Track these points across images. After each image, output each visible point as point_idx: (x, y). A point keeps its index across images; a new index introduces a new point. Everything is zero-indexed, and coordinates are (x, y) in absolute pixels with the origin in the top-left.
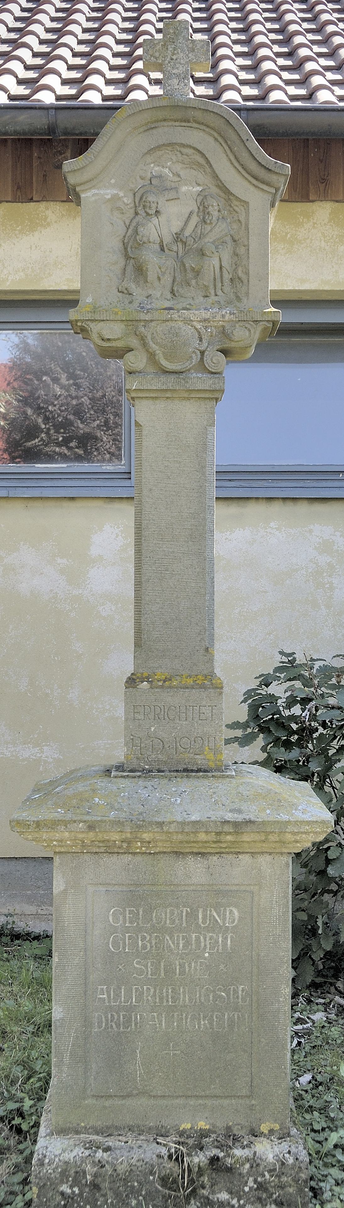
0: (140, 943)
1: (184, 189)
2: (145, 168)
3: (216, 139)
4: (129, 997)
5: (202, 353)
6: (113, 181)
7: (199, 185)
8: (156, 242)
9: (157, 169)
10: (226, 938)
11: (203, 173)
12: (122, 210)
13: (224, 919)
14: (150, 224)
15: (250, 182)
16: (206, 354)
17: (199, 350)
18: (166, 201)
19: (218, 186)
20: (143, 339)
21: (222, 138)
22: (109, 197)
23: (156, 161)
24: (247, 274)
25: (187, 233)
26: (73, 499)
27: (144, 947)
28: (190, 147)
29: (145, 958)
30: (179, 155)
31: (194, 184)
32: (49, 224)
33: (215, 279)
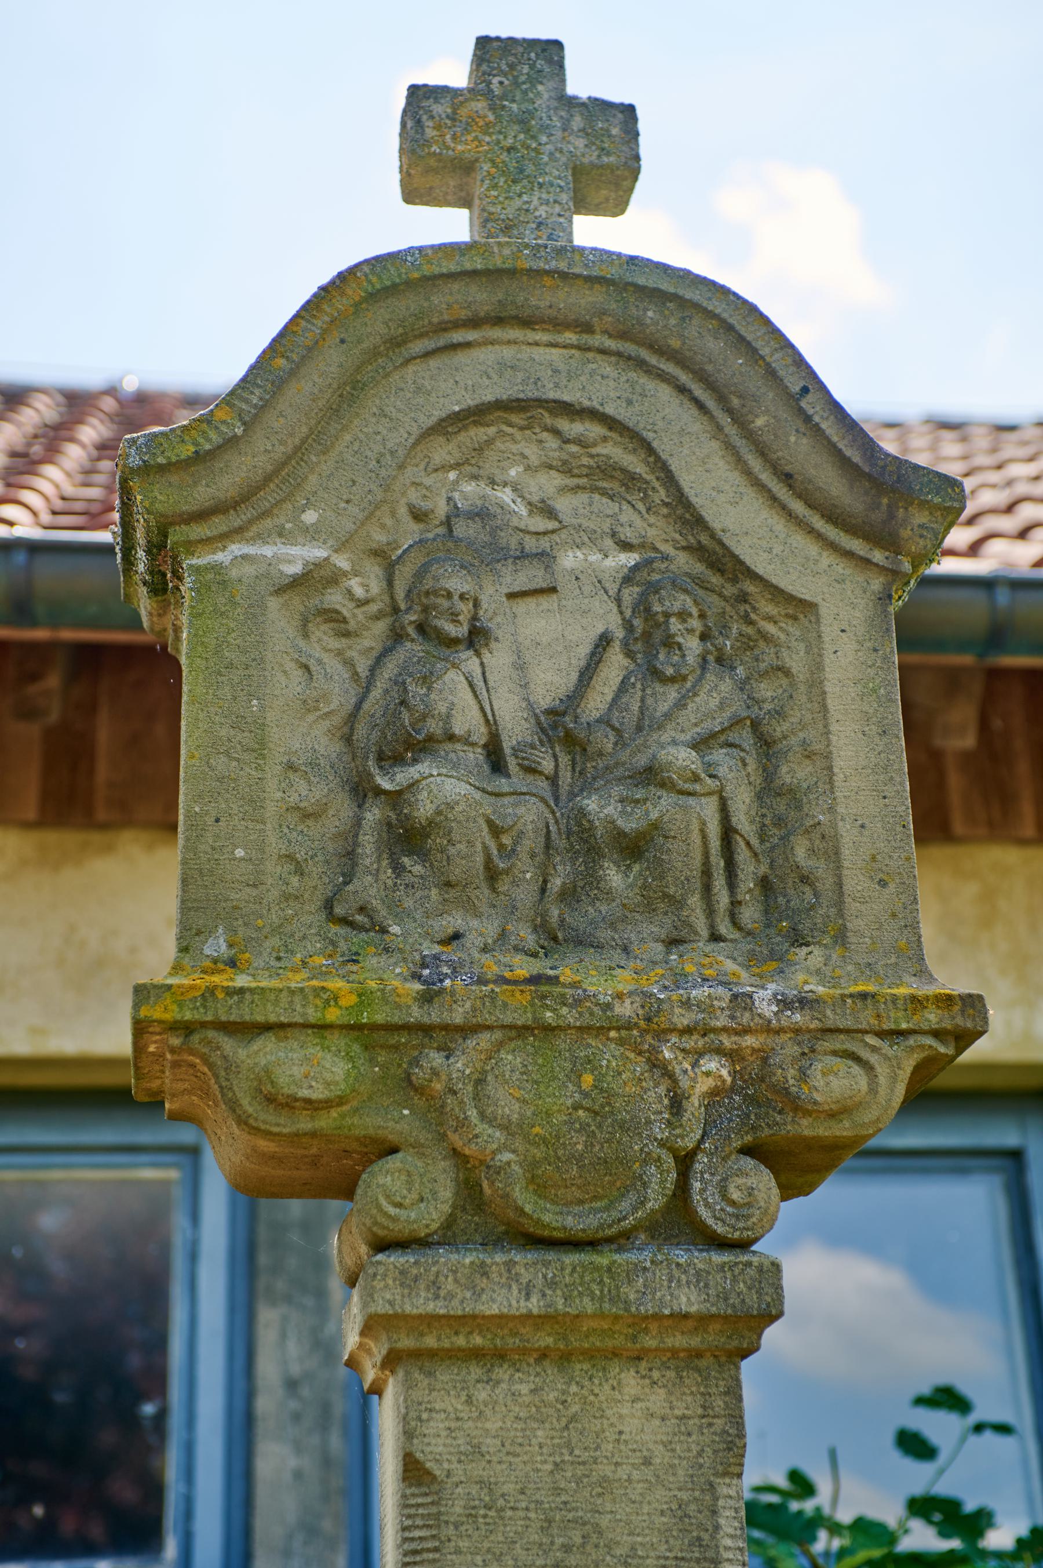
1: (570, 559)
2: (428, 481)
3: (682, 390)
5: (685, 1162)
6: (310, 517)
7: (626, 546)
8: (474, 738)
9: (469, 488)
11: (640, 506)
12: (345, 621)
14: (451, 675)
15: (818, 536)
16: (698, 1167)
17: (670, 1149)
18: (512, 596)
19: (698, 550)
22: (295, 569)
23: (467, 462)
24: (834, 856)
31: (609, 542)
33: (707, 873)
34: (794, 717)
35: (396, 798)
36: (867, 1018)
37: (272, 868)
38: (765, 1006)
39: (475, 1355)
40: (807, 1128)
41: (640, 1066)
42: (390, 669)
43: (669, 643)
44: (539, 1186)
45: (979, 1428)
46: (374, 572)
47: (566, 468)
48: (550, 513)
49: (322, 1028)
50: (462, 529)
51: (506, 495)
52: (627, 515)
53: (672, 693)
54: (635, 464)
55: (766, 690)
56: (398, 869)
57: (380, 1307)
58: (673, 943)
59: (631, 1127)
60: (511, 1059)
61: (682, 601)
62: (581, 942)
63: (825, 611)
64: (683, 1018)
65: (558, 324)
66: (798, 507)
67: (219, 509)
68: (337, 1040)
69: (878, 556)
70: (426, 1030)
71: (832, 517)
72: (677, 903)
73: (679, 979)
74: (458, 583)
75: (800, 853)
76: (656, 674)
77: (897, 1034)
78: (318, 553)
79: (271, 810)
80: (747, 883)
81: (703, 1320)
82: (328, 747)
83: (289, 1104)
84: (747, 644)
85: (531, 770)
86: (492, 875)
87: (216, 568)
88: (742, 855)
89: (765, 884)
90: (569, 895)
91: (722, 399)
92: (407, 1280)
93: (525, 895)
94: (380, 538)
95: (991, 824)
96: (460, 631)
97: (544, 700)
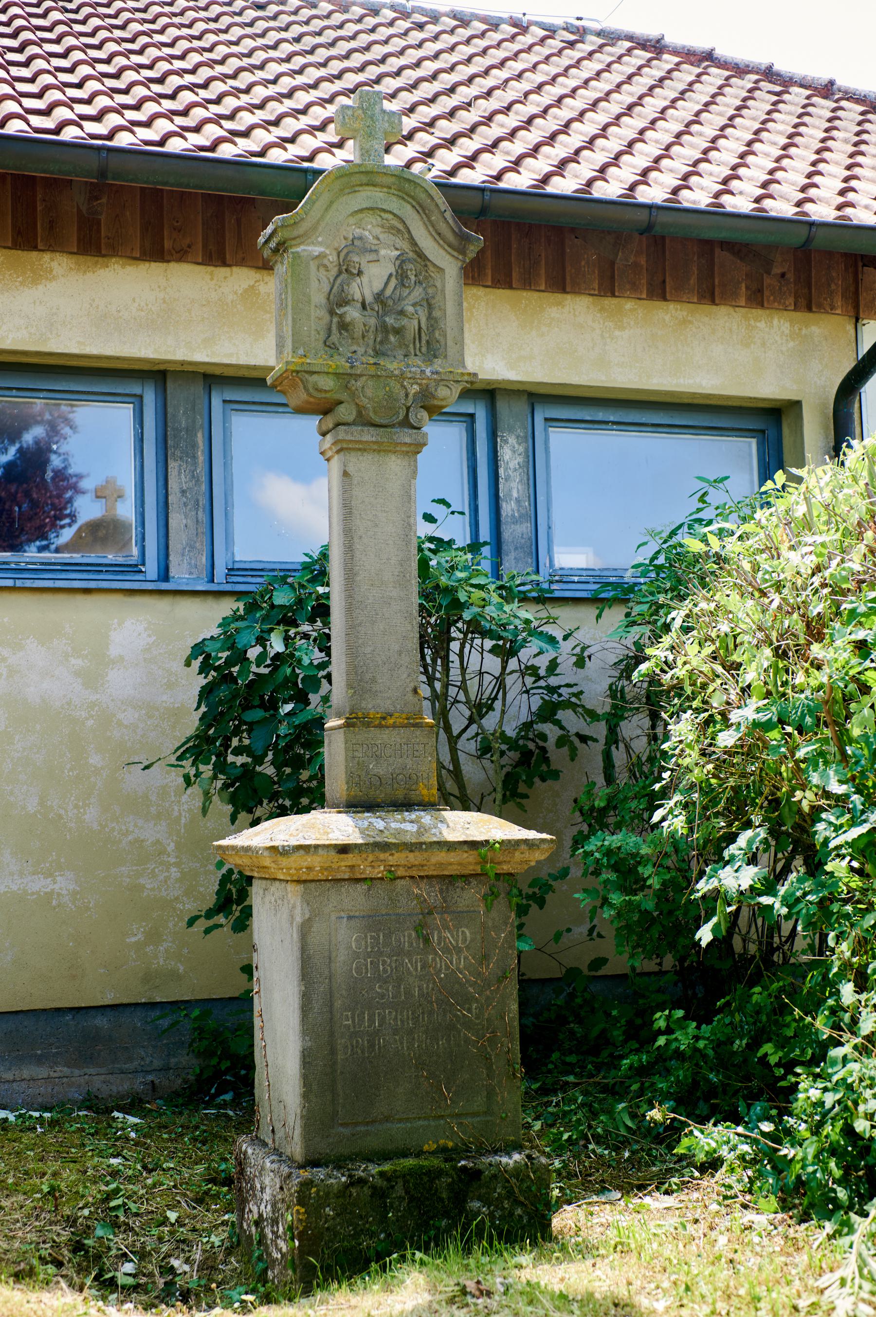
0: (381, 968)
1: (383, 252)
3: (413, 206)
4: (371, 1020)
6: (320, 239)
7: (397, 249)
9: (358, 230)
10: (460, 959)
13: (457, 942)
19: (415, 252)
20: (353, 395)
21: (422, 209)
22: (316, 254)
24: (445, 336)
25: (388, 292)
26: (87, 591)
27: (385, 971)
28: (390, 212)
29: (386, 982)
30: (379, 219)
32: (54, 278)
34: (437, 298)
35: (341, 316)
36: (451, 377)
37: (313, 333)
38: (428, 373)
39: (360, 449)
40: (436, 402)
41: (399, 386)
42: (339, 281)
43: (407, 277)
44: (375, 412)
45: (453, 513)
46: (335, 254)
47: (383, 226)
48: (378, 239)
49: (328, 373)
50: (356, 243)
51: (367, 233)
52: (398, 241)
53: (407, 291)
54: (401, 227)
55: (430, 291)
56: (341, 334)
57: (340, 438)
58: (406, 356)
59: (396, 400)
60: (370, 383)
61: (411, 266)
62: (384, 354)
63: (447, 271)
64: (409, 375)
65: (382, 186)
66: (441, 242)
67: (298, 237)
68: (331, 376)
69: (460, 257)
70: (351, 375)
71: (450, 246)
72: (407, 346)
73: (408, 366)
74: (356, 259)
75: (437, 335)
76: (404, 285)
77: (458, 381)
78: (322, 249)
79: (312, 318)
80: (424, 342)
81: (410, 444)
82: (324, 301)
83: (318, 390)
84: (426, 278)
85: (372, 309)
86: (363, 337)
87: (297, 253)
88: (423, 334)
89: (428, 342)
90: (381, 343)
91: (424, 210)
92: (346, 432)
93: (371, 342)
94: (336, 245)
95: (473, 278)
96: (356, 272)
97: (376, 291)
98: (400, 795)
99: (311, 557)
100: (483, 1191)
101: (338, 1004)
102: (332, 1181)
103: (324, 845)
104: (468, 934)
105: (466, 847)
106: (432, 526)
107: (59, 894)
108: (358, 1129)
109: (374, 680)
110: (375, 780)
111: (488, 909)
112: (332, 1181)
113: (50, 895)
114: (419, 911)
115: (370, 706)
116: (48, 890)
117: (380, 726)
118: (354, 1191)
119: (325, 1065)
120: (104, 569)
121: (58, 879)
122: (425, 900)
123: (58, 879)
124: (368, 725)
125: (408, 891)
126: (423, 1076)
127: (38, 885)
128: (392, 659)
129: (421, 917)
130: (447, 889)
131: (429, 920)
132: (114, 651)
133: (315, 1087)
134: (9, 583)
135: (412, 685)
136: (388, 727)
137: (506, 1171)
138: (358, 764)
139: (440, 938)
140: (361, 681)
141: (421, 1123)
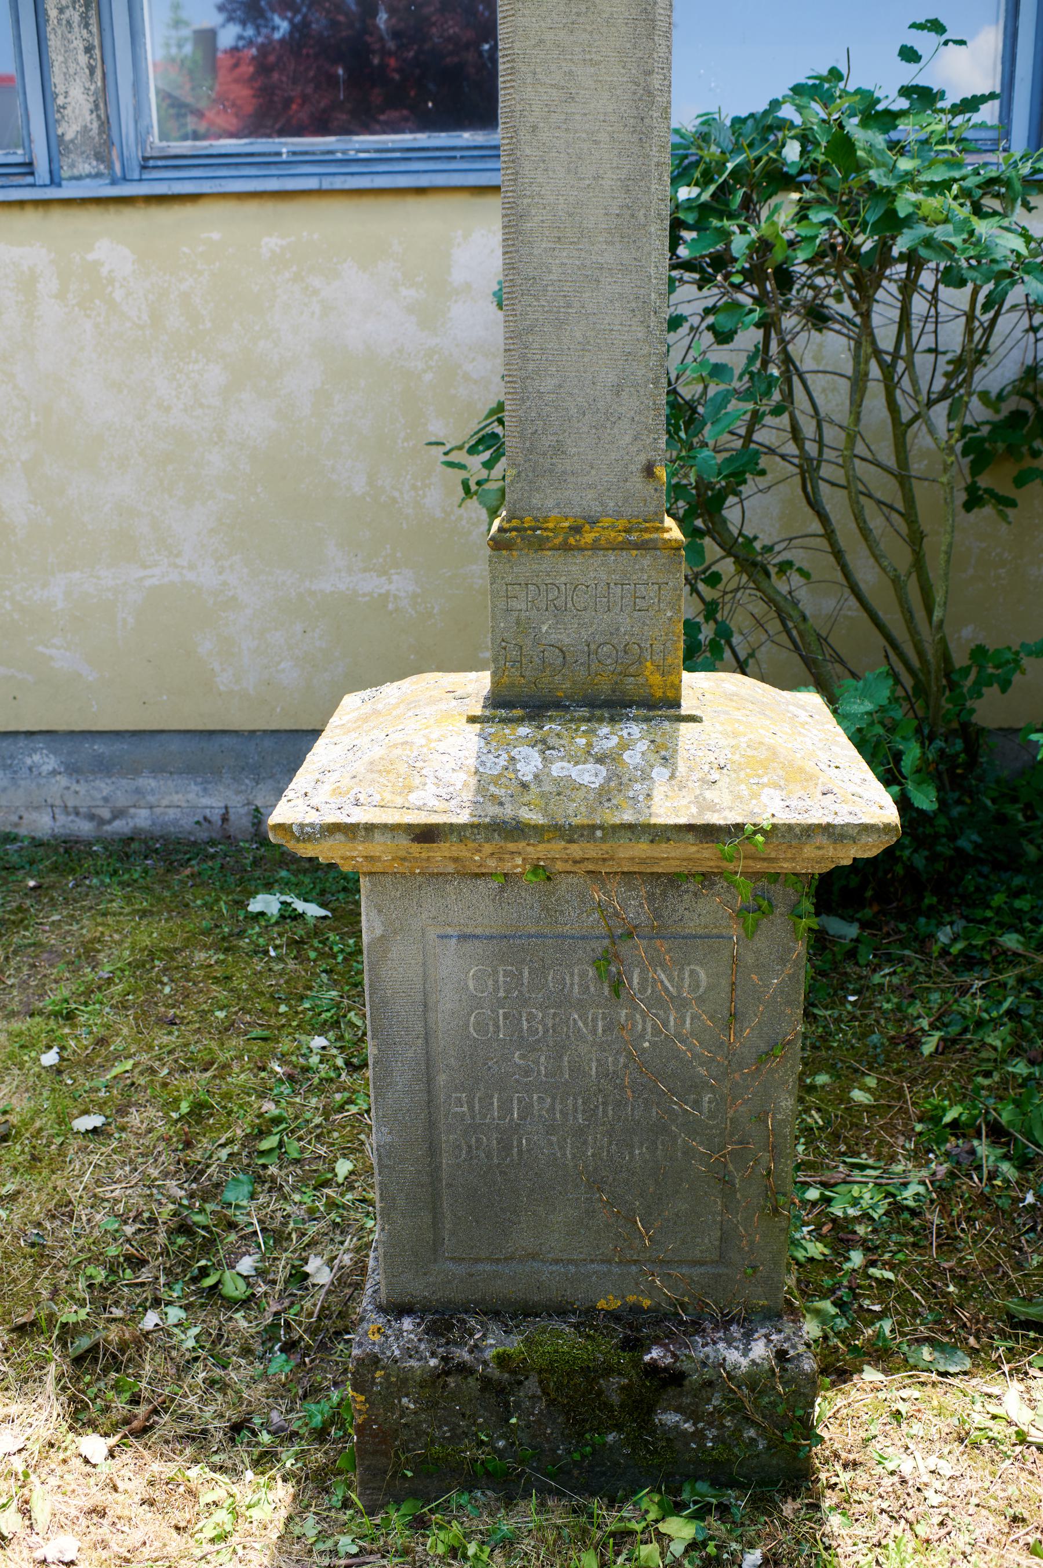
0: (525, 1024)
4: (506, 1108)
13: (679, 988)
27: (533, 1031)
98: (604, 686)
99: (682, 137)
100: (687, 1400)
101: (442, 1079)
102: (413, 1363)
103: (385, 826)
104: (702, 975)
105: (690, 837)
106: (913, 67)
107: (396, 597)
108: (480, 1267)
109: (559, 449)
110: (553, 656)
111: (750, 934)
112: (413, 1363)
113: (385, 597)
114: (604, 931)
115: (550, 503)
116: (383, 591)
117: (566, 548)
118: (452, 1381)
119: (419, 1172)
120: (458, 154)
121: (395, 577)
122: (616, 914)
123: (395, 577)
124: (540, 545)
125: (582, 896)
126: (601, 1200)
127: (372, 584)
128: (601, 404)
129: (606, 942)
130: (664, 894)
131: (624, 949)
132: (458, 276)
133: (401, 1202)
134: (312, 184)
135: (642, 459)
136: (582, 549)
137: (730, 1377)
138: (518, 623)
139: (644, 981)
140: (530, 451)
141: (594, 1266)
